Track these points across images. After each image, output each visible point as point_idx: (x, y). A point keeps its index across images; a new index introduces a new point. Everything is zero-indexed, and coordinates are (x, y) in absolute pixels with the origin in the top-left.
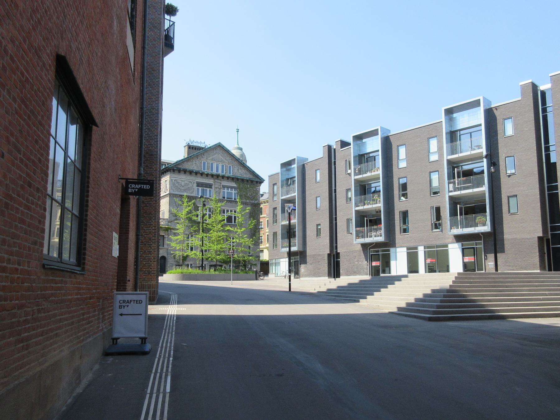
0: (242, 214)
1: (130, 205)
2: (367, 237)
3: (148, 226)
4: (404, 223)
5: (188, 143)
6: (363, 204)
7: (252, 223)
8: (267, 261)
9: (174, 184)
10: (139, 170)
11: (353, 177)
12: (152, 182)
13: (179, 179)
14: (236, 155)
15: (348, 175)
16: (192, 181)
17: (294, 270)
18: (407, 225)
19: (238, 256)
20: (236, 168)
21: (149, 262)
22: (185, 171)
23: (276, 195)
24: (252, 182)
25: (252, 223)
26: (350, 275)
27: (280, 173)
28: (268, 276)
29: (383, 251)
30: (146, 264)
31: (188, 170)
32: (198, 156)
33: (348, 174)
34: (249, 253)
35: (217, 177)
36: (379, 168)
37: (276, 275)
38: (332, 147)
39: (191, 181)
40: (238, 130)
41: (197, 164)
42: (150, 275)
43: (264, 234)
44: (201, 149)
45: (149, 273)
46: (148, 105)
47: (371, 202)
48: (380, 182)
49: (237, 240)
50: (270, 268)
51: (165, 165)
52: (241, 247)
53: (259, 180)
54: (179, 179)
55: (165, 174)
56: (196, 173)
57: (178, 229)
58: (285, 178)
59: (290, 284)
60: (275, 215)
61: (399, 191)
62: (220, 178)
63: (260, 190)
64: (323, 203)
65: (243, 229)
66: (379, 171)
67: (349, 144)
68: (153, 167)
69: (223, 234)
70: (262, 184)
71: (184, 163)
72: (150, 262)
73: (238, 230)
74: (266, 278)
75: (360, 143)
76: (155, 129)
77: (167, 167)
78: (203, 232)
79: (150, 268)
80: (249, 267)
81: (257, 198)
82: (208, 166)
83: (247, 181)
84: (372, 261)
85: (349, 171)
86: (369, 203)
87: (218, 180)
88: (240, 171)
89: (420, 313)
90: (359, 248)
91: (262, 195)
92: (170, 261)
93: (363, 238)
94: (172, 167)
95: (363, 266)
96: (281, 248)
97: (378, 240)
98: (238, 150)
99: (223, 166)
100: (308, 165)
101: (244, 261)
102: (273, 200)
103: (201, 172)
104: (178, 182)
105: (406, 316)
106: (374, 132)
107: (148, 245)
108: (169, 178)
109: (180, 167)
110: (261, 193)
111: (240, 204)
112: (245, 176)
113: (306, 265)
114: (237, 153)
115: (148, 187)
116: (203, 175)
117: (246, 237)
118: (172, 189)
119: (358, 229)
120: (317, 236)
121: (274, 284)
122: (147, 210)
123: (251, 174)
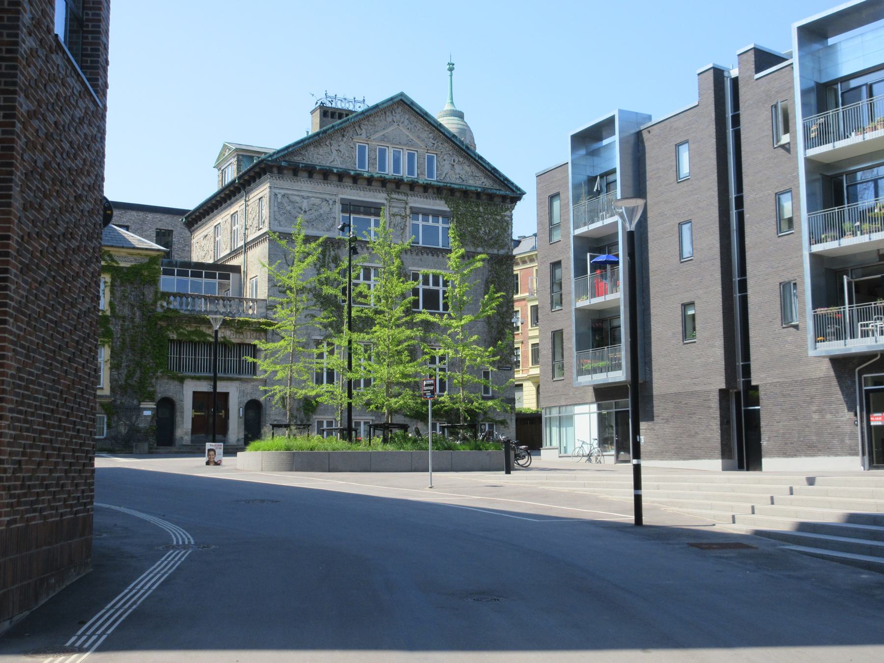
2: (853, 336)
5: (322, 103)
7: (492, 299)
8: (531, 414)
9: (280, 206)
11: (801, 154)
13: (295, 193)
14: (446, 126)
15: (782, 151)
16: (330, 197)
19: (452, 399)
20: (446, 162)
23: (558, 225)
24: (491, 197)
25: (492, 299)
27: (570, 165)
28: (540, 455)
31: (318, 168)
32: (343, 129)
33: (783, 146)
34: (486, 390)
35: (396, 184)
37: (562, 451)
38: (726, 74)
39: (327, 197)
40: (453, 65)
43: (522, 343)
49: (449, 351)
50: (546, 432)
52: (461, 370)
53: (508, 193)
54: (295, 193)
55: (257, 181)
56: (341, 176)
58: (583, 178)
59: (638, 499)
60: (556, 284)
62: (403, 188)
63: (512, 219)
64: (843, 130)
65: (467, 319)
73: (452, 321)
74: (536, 461)
75: (819, 50)
77: (262, 161)
78: (350, 328)
80: (487, 429)
81: (503, 240)
82: (371, 155)
83: (478, 195)
84: (869, 413)
85: (785, 139)
87: (398, 193)
88: (458, 168)
90: (826, 369)
91: (518, 243)
94: (276, 159)
95: (839, 427)
96: (575, 375)
99: (411, 157)
100: (651, 133)
101: (470, 412)
102: (550, 240)
103: (352, 173)
104: (291, 201)
108: (268, 190)
109: (297, 159)
110: (515, 237)
111: (456, 243)
112: (471, 182)
113: (650, 423)
116: (360, 181)
117: (476, 342)
118: (275, 219)
119: (821, 311)
120: (685, 337)
123: (487, 176)
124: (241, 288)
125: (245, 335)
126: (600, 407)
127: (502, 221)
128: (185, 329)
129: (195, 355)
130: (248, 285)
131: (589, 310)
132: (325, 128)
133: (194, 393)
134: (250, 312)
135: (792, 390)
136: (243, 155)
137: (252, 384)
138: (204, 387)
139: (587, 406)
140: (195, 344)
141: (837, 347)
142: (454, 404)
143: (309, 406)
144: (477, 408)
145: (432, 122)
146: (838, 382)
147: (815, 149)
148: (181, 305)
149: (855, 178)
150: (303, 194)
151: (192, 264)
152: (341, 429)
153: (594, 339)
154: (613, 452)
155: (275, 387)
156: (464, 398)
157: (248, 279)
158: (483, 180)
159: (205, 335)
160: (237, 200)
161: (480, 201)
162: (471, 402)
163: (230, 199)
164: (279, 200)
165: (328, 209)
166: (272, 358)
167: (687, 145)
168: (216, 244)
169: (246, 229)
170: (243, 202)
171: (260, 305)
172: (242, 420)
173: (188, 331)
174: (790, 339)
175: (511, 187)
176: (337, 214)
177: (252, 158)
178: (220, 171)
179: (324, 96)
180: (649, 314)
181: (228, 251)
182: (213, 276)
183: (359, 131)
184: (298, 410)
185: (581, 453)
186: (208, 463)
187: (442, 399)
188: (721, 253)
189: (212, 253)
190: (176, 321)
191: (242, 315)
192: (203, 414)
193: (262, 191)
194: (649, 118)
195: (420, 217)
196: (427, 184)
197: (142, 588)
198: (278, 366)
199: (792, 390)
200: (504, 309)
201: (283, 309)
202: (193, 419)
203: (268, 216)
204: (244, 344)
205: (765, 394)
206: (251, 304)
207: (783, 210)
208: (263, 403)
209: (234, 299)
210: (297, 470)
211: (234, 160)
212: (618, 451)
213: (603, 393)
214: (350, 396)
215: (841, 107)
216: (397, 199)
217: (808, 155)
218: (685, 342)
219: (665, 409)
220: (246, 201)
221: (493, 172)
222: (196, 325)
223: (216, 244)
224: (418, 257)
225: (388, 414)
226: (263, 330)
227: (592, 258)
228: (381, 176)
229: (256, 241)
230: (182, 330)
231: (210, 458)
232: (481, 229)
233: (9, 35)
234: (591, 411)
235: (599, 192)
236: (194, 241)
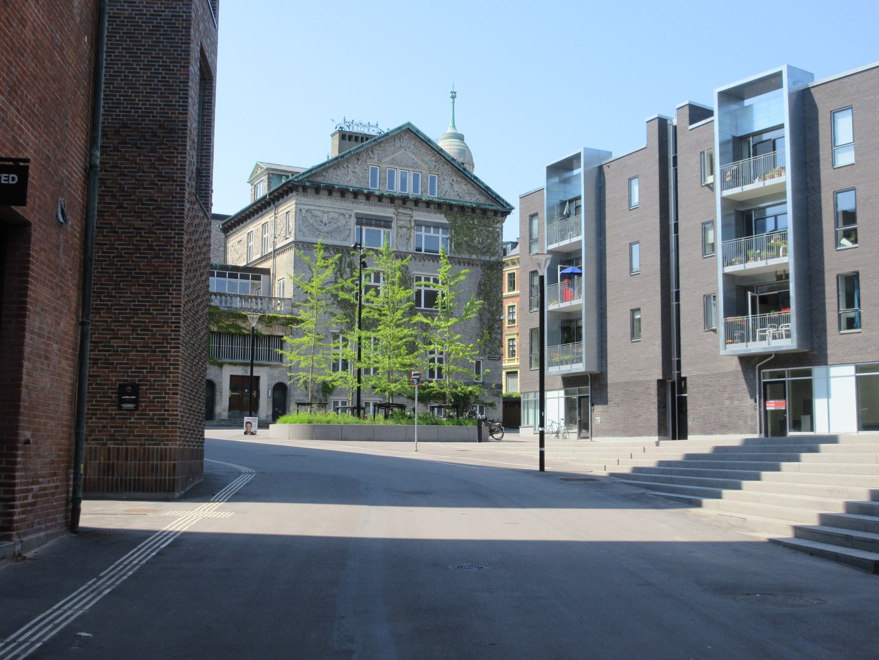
0: (450, 286)
1: (29, 241)
2: (754, 340)
3: (160, 306)
4: (850, 304)
5: (341, 127)
6: (743, 259)
9: (304, 219)
10: (90, 155)
12: (21, 164)
15: (707, 189)
16: (347, 212)
17: (578, 419)
18: (856, 308)
20: (446, 182)
21: (161, 393)
22: (330, 190)
23: (537, 240)
24: (484, 211)
26: (712, 434)
28: (519, 432)
29: (794, 374)
30: (156, 400)
33: (708, 185)
36: (783, 168)
38: (669, 122)
39: (344, 212)
40: (455, 93)
41: (357, 172)
42: (165, 428)
43: (518, 334)
44: (365, 139)
45: (163, 420)
46: (165, 8)
47: (764, 253)
48: (785, 203)
50: (524, 413)
51: (287, 177)
53: (500, 208)
55: (285, 197)
56: (356, 194)
57: (302, 321)
58: (557, 201)
59: (542, 454)
61: (837, 225)
62: (409, 204)
63: (502, 231)
66: (785, 175)
67: (710, 113)
68: (175, 160)
69: (406, 331)
70: (508, 216)
71: (329, 171)
72: (166, 393)
73: (441, 323)
74: (508, 436)
75: (736, 110)
76: (181, 67)
77: (289, 182)
78: (360, 328)
79: (165, 410)
81: (494, 249)
83: (473, 210)
84: (765, 400)
85: (710, 180)
86: (759, 255)
87: (404, 208)
88: (456, 187)
89: (853, 547)
90: (735, 365)
92: (296, 393)
93: (742, 341)
95: (743, 411)
97: (782, 347)
98: (454, 140)
99: (416, 177)
100: (611, 168)
101: (456, 396)
103: (366, 191)
105: (812, 553)
106: (773, 80)
107: (159, 352)
108: (294, 206)
109: (319, 179)
111: (445, 261)
112: (467, 199)
113: (605, 406)
114: (448, 147)
115: (13, 179)
116: (371, 199)
118: (300, 231)
119: (731, 319)
120: (633, 336)
121: (513, 453)
122: (159, 266)
123: (481, 193)
124: (270, 289)
125: (274, 328)
126: (566, 393)
127: (493, 232)
128: (223, 323)
129: (232, 345)
130: (277, 285)
131: (559, 312)
132: (343, 153)
133: (231, 376)
134: (278, 308)
135: (710, 381)
136: (274, 174)
137: (279, 369)
138: (239, 371)
139: (556, 392)
140: (232, 335)
141: (741, 348)
142: (441, 388)
143: (327, 389)
144: (459, 392)
145: (435, 148)
146: (744, 375)
147: (732, 189)
148: (221, 302)
149: (765, 213)
150: (323, 209)
151: (230, 267)
152: (352, 408)
153: (563, 337)
154: (576, 430)
155: (300, 373)
156: (450, 384)
157: (277, 281)
158: (478, 197)
159: (239, 328)
160: (268, 212)
161: (474, 215)
162: (456, 387)
163: (261, 211)
164: (303, 215)
165: (344, 222)
166: (298, 350)
167: (637, 179)
168: (249, 249)
169: (275, 237)
170: (273, 214)
171: (287, 303)
172: (271, 399)
173: (226, 325)
174: (710, 340)
175: (502, 203)
176: (352, 226)
177: (280, 176)
178: (253, 186)
179: (343, 121)
180: (606, 317)
181: (259, 256)
182: (247, 277)
183: (371, 155)
184: (317, 391)
185: (551, 430)
186: (246, 433)
187: (431, 384)
188: (662, 269)
189: (245, 256)
190: (217, 316)
191: (272, 311)
192: (238, 394)
193: (289, 206)
194: (610, 153)
195: (423, 228)
196: (429, 200)
197: (236, 485)
198: (302, 357)
199: (710, 381)
200: (494, 308)
201: (306, 312)
202: (230, 398)
203: (294, 228)
204: (272, 336)
205: (691, 384)
206: (279, 302)
207: (708, 238)
208: (288, 386)
209: (265, 298)
210: (316, 439)
211: (265, 178)
212: (580, 431)
213: (569, 381)
214: (359, 381)
215: (752, 158)
216: (403, 214)
217: (723, 195)
218: (633, 341)
219: (617, 395)
220: (275, 214)
221: (486, 190)
222: (233, 319)
223: (249, 249)
224: (420, 263)
225: (389, 396)
226: (290, 322)
227: (562, 269)
228: (390, 195)
229: (284, 249)
230: (221, 324)
231: (247, 429)
232: (475, 239)
233: (180, 206)
234: (560, 396)
235: (568, 216)
236: (229, 245)
